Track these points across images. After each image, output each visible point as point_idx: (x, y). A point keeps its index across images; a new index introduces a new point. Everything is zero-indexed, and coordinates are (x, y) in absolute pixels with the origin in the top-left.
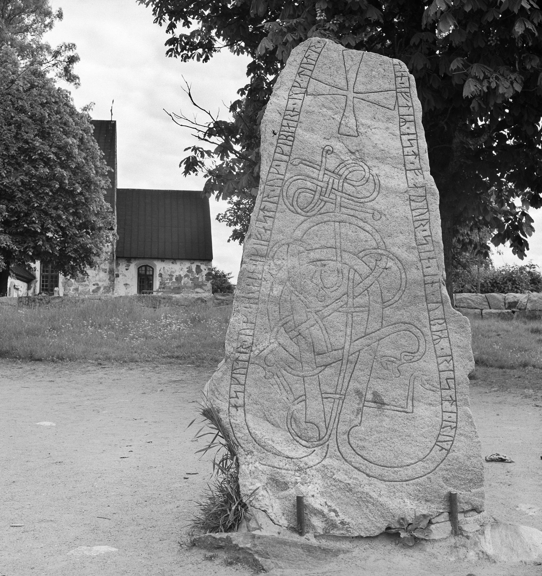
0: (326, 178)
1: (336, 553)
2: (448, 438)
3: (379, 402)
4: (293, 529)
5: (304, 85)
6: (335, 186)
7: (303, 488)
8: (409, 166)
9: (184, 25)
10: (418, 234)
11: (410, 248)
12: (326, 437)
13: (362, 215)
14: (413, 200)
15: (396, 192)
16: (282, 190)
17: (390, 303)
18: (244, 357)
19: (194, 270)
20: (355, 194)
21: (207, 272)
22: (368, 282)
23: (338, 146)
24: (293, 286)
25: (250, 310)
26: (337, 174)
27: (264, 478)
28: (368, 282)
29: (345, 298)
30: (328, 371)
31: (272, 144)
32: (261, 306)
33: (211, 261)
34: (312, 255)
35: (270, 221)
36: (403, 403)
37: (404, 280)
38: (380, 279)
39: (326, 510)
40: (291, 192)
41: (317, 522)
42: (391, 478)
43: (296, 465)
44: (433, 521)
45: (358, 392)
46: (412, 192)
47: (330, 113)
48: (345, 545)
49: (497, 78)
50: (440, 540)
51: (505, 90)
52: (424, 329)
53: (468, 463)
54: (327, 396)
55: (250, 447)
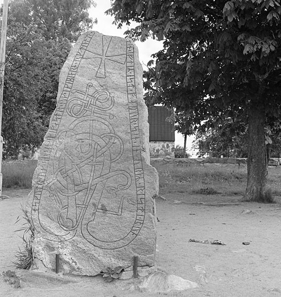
0: (88, 99)
1: (69, 282)
2: (138, 229)
3: (104, 209)
4: (53, 270)
5: (82, 54)
6: (92, 103)
7: (61, 251)
8: (129, 92)
9: (127, 24)
10: (132, 126)
11: (127, 133)
12: (76, 226)
13: (104, 117)
14: (131, 109)
15: (122, 105)
16: (66, 106)
17: (114, 160)
18: (40, 186)
19: (166, 146)
20: (101, 107)
21: (172, 147)
22: (104, 150)
23: (95, 83)
24: (66, 152)
25: (45, 164)
26: (94, 97)
27: (43, 245)
28: (104, 150)
29: (92, 158)
30: (80, 194)
31: (63, 83)
32: (50, 161)
33: (174, 141)
34: (78, 137)
35: (59, 120)
36: (116, 210)
37: (122, 149)
38: (110, 148)
39: (71, 262)
40: (70, 106)
41: (66, 267)
42: (106, 247)
43: (59, 239)
44: (125, 270)
45: (94, 204)
46: (130, 105)
47: (92, 67)
48: (78, 279)
49: (262, 43)
50: (126, 280)
51: (266, 49)
52: (131, 173)
53: (146, 242)
54: (79, 206)
55: (39, 229)
